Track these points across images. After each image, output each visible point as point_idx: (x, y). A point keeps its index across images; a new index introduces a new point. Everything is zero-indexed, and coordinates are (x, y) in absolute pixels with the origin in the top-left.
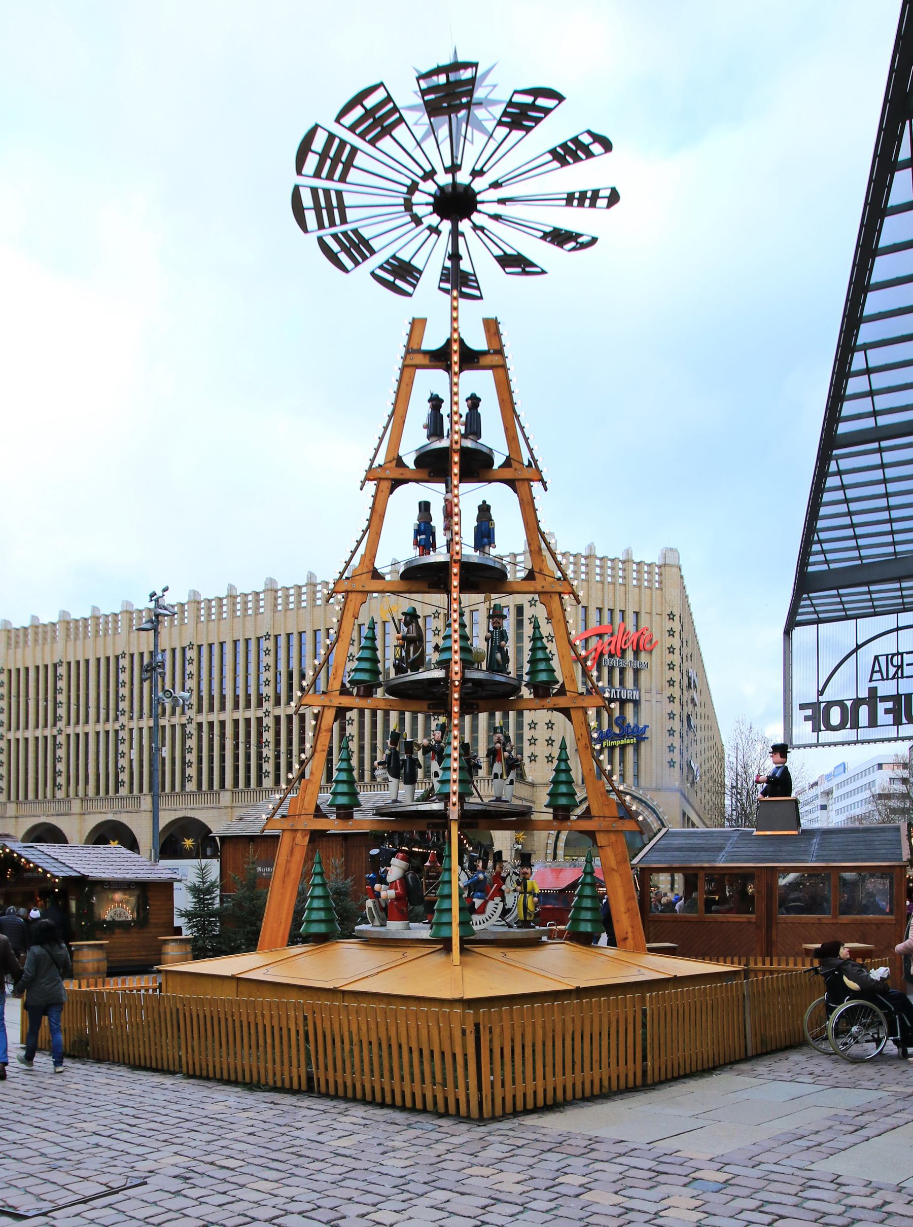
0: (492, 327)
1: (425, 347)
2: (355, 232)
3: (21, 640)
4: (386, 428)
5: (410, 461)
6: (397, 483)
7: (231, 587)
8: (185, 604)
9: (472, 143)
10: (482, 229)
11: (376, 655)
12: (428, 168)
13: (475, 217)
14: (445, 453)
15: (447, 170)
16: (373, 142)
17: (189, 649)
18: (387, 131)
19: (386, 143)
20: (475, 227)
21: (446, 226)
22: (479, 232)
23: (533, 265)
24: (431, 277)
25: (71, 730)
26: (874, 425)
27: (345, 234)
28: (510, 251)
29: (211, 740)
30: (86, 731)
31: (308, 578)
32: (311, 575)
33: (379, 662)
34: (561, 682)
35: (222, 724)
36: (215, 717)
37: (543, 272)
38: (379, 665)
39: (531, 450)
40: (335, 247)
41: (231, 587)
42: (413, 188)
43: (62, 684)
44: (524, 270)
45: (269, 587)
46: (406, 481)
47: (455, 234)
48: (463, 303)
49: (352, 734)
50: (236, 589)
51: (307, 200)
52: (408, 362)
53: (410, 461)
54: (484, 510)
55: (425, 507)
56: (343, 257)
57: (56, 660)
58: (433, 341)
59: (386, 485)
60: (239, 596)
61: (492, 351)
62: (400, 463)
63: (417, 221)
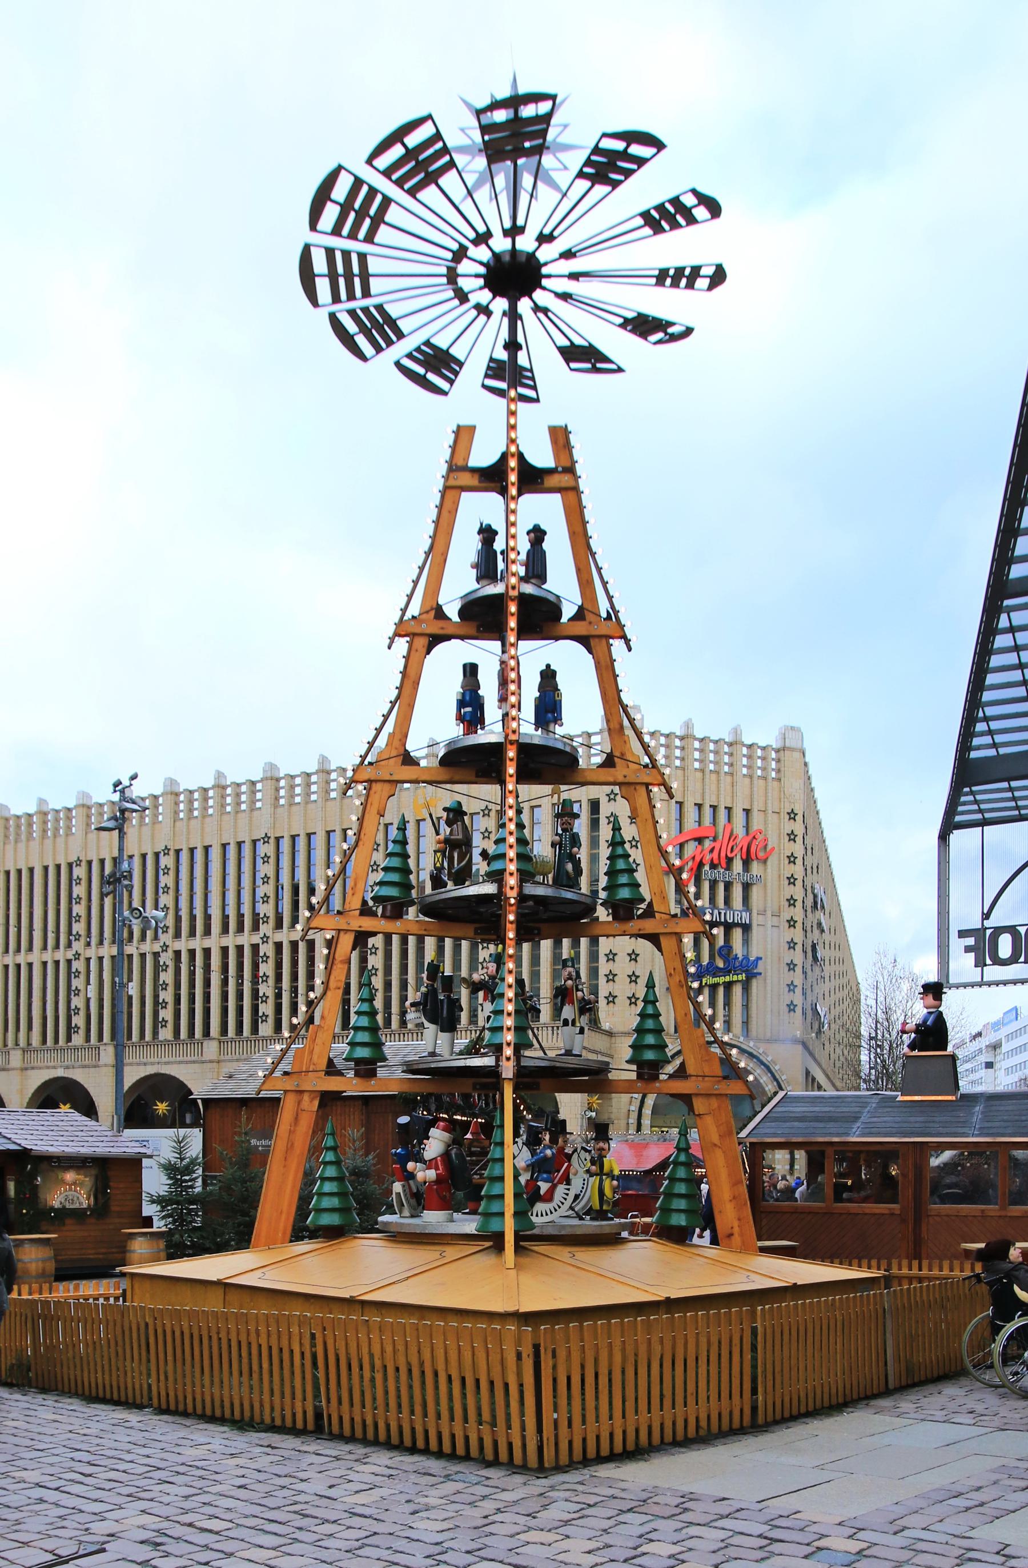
1: (473, 463)
4: (421, 569)
5: (452, 611)
6: (435, 640)
10: (545, 311)
13: (539, 295)
14: (497, 602)
15: (506, 233)
16: (412, 192)
18: (432, 178)
19: (430, 194)
20: (537, 309)
21: (500, 305)
24: (473, 372)
28: (578, 341)
34: (648, 900)
39: (610, 598)
42: (460, 254)
44: (594, 366)
45: (269, 775)
46: (447, 638)
47: (513, 316)
51: (320, 264)
52: (452, 482)
53: (452, 611)
54: (548, 676)
55: (471, 671)
59: (421, 642)
60: (229, 786)
62: (439, 613)
63: (462, 297)
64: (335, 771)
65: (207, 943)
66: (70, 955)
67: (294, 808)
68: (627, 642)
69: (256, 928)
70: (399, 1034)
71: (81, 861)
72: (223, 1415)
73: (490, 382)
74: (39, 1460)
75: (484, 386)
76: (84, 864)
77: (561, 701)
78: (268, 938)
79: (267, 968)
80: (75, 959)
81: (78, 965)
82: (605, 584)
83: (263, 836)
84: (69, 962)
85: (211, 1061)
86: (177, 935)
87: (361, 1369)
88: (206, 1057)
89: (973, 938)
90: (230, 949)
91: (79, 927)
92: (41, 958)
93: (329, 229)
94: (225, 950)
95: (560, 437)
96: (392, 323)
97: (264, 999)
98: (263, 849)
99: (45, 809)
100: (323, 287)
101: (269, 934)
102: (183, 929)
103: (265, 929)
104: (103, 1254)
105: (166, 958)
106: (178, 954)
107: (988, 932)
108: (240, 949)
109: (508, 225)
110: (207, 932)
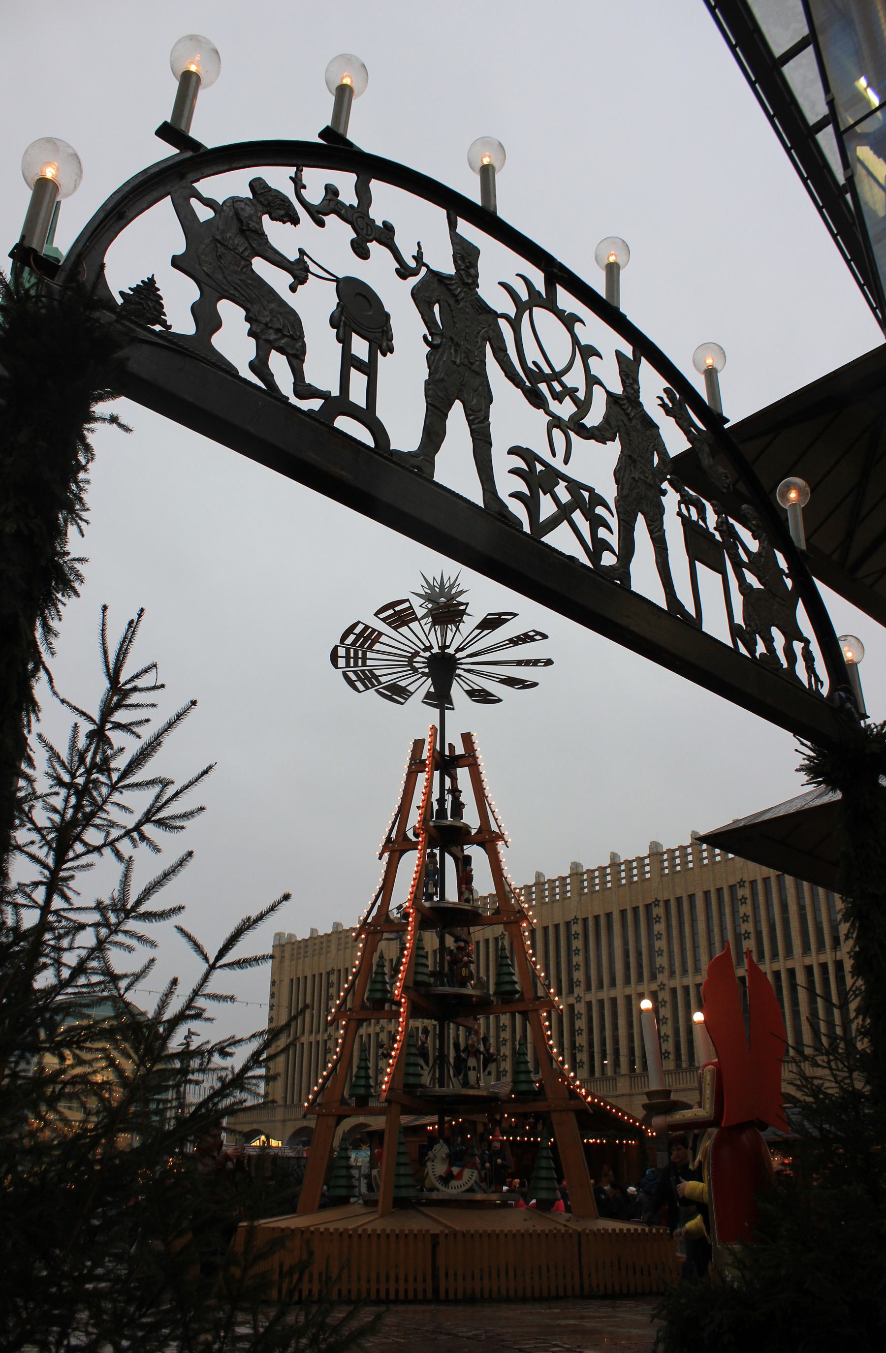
2: (370, 671)
7: (539, 875)
8: (532, 886)
12: (428, 644)
16: (395, 628)
17: (574, 923)
18: (405, 623)
19: (404, 630)
25: (592, 997)
27: (363, 672)
28: (476, 687)
29: (602, 1028)
30: (600, 998)
31: (611, 859)
32: (614, 856)
35: (614, 1001)
36: (605, 995)
37: (499, 700)
40: (354, 677)
41: (539, 875)
42: (416, 654)
43: (578, 944)
45: (575, 871)
49: (666, 1017)
50: (544, 876)
51: (342, 652)
56: (358, 684)
57: (569, 918)
60: (665, 853)
64: (665, 853)
65: (823, 958)
66: (378, 1029)
67: (556, 904)
68: (506, 842)
69: (653, 977)
70: (675, 1073)
71: (577, 919)
76: (580, 922)
78: (581, 998)
79: (581, 1024)
80: (660, 990)
81: (580, 1008)
82: (493, 812)
83: (654, 900)
84: (326, 1041)
85: (623, 1095)
86: (588, 988)
88: (619, 1092)
90: (797, 970)
91: (579, 975)
92: (803, 962)
94: (809, 969)
95: (467, 738)
96: (376, 678)
97: (665, 1038)
98: (741, 893)
99: (542, 880)
100: (342, 662)
101: (666, 982)
102: (563, 987)
103: (662, 978)
105: (580, 1008)
106: (674, 991)
108: (686, 989)
110: (613, 983)
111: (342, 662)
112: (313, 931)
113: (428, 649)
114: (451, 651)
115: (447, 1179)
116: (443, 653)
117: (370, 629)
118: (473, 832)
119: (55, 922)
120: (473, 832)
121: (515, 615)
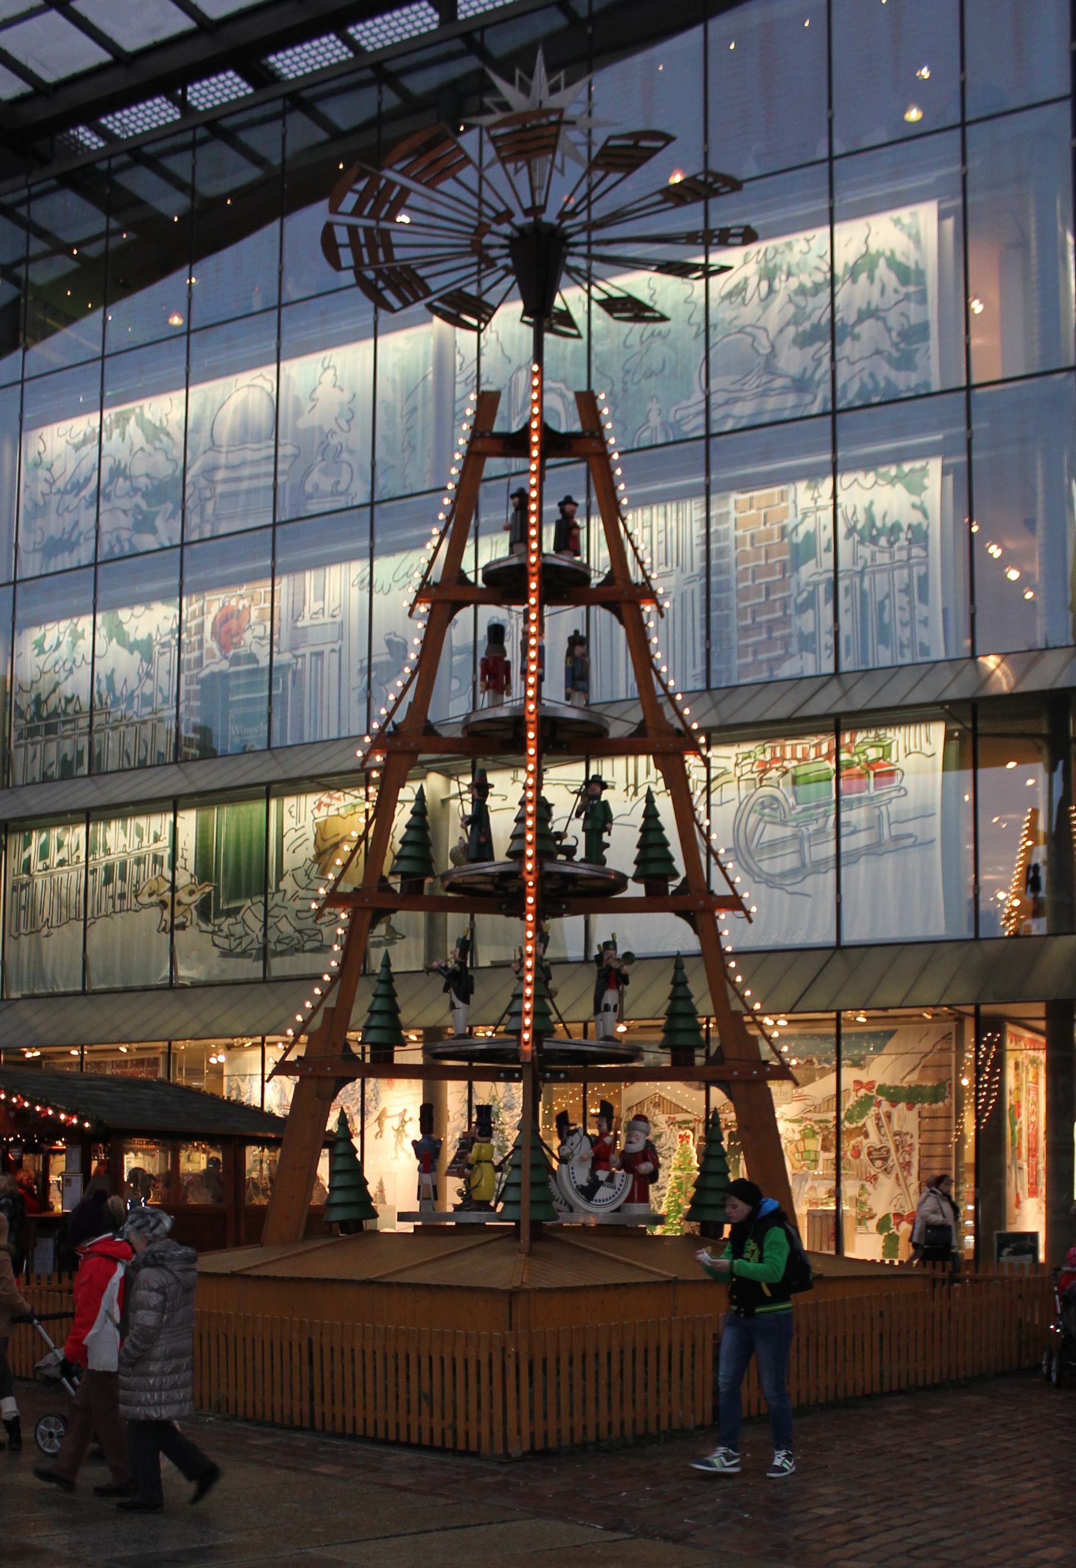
0: (586, 402)
3: (945, 1316)
6: (380, 914)
9: (562, 172)
11: (427, 836)
12: (501, 208)
15: (527, 212)
22: (574, 275)
23: (650, 309)
26: (476, 916)
33: (326, 1009)
38: (333, 1004)
48: (548, 337)
51: (342, 236)
54: (578, 642)
55: (497, 632)
58: (507, 422)
61: (587, 434)
62: (383, 885)
72: (409, 1439)
73: (526, 319)
74: (30, 759)
75: (522, 321)
77: (566, 687)
87: (597, 1399)
89: (396, 1062)
93: (349, 209)
95: (586, 402)
96: (421, 280)
100: (346, 257)
104: (1050, 1360)
107: (410, 1055)
109: (527, 204)
111: (346, 257)
112: (492, 786)
113: (506, 216)
114: (549, 217)
115: (589, 1192)
116: (538, 226)
117: (366, 212)
118: (596, 580)
119: (287, 1051)
120: (596, 580)
121: (668, 139)
